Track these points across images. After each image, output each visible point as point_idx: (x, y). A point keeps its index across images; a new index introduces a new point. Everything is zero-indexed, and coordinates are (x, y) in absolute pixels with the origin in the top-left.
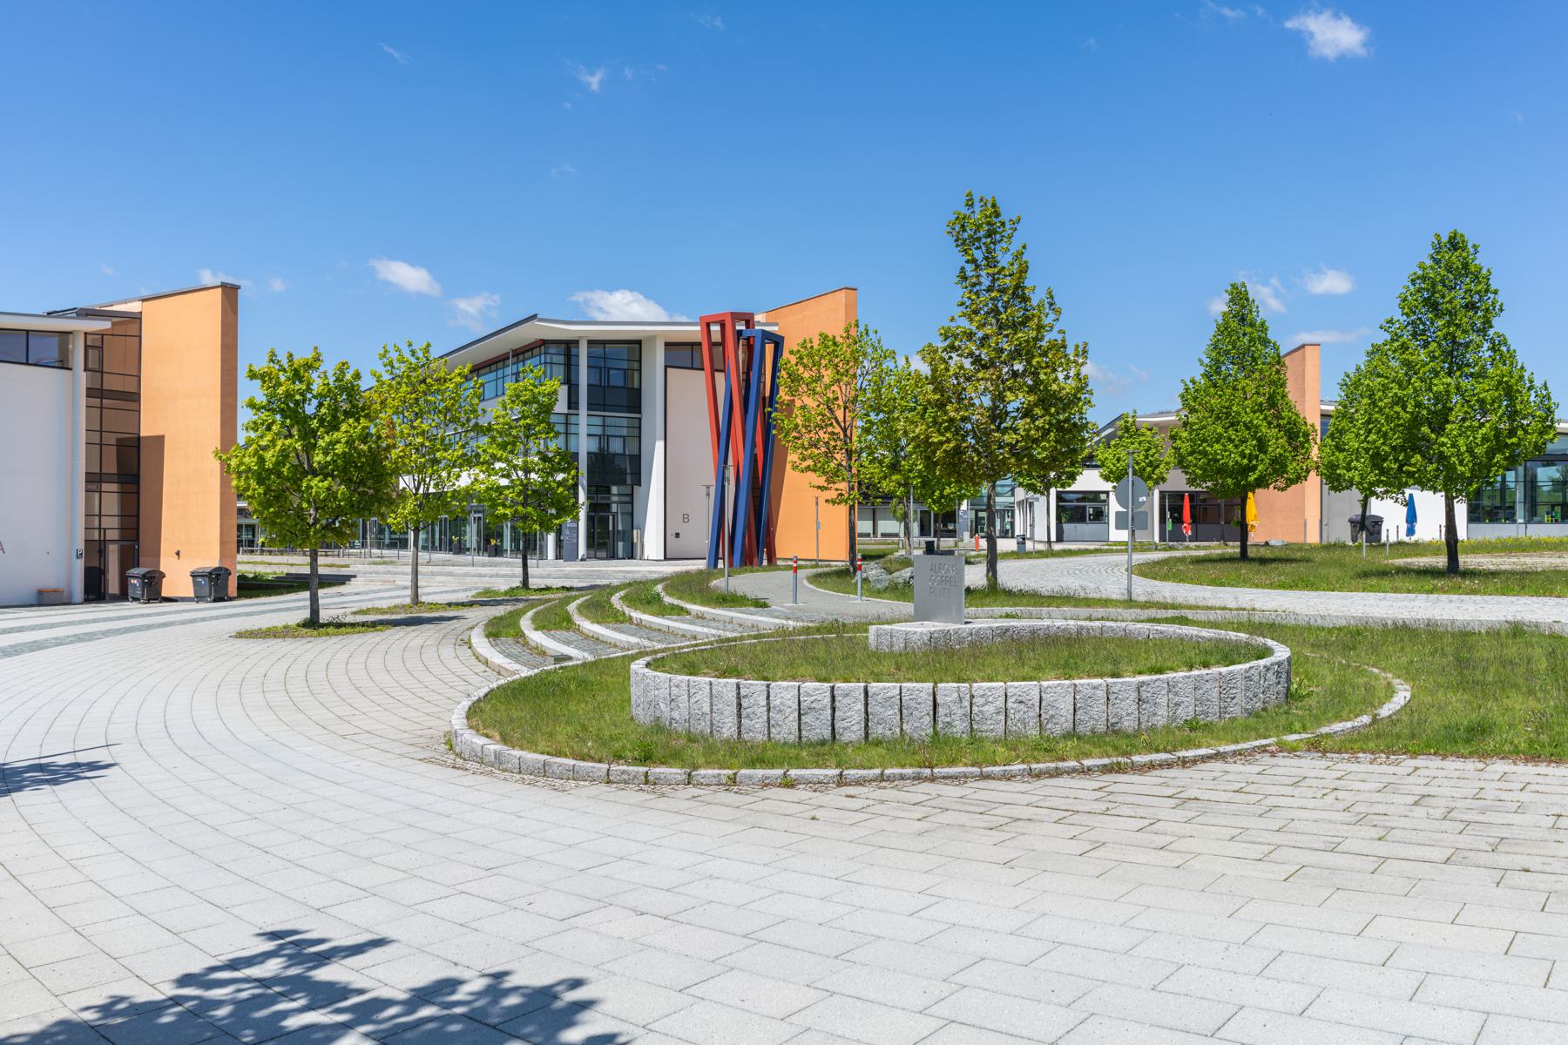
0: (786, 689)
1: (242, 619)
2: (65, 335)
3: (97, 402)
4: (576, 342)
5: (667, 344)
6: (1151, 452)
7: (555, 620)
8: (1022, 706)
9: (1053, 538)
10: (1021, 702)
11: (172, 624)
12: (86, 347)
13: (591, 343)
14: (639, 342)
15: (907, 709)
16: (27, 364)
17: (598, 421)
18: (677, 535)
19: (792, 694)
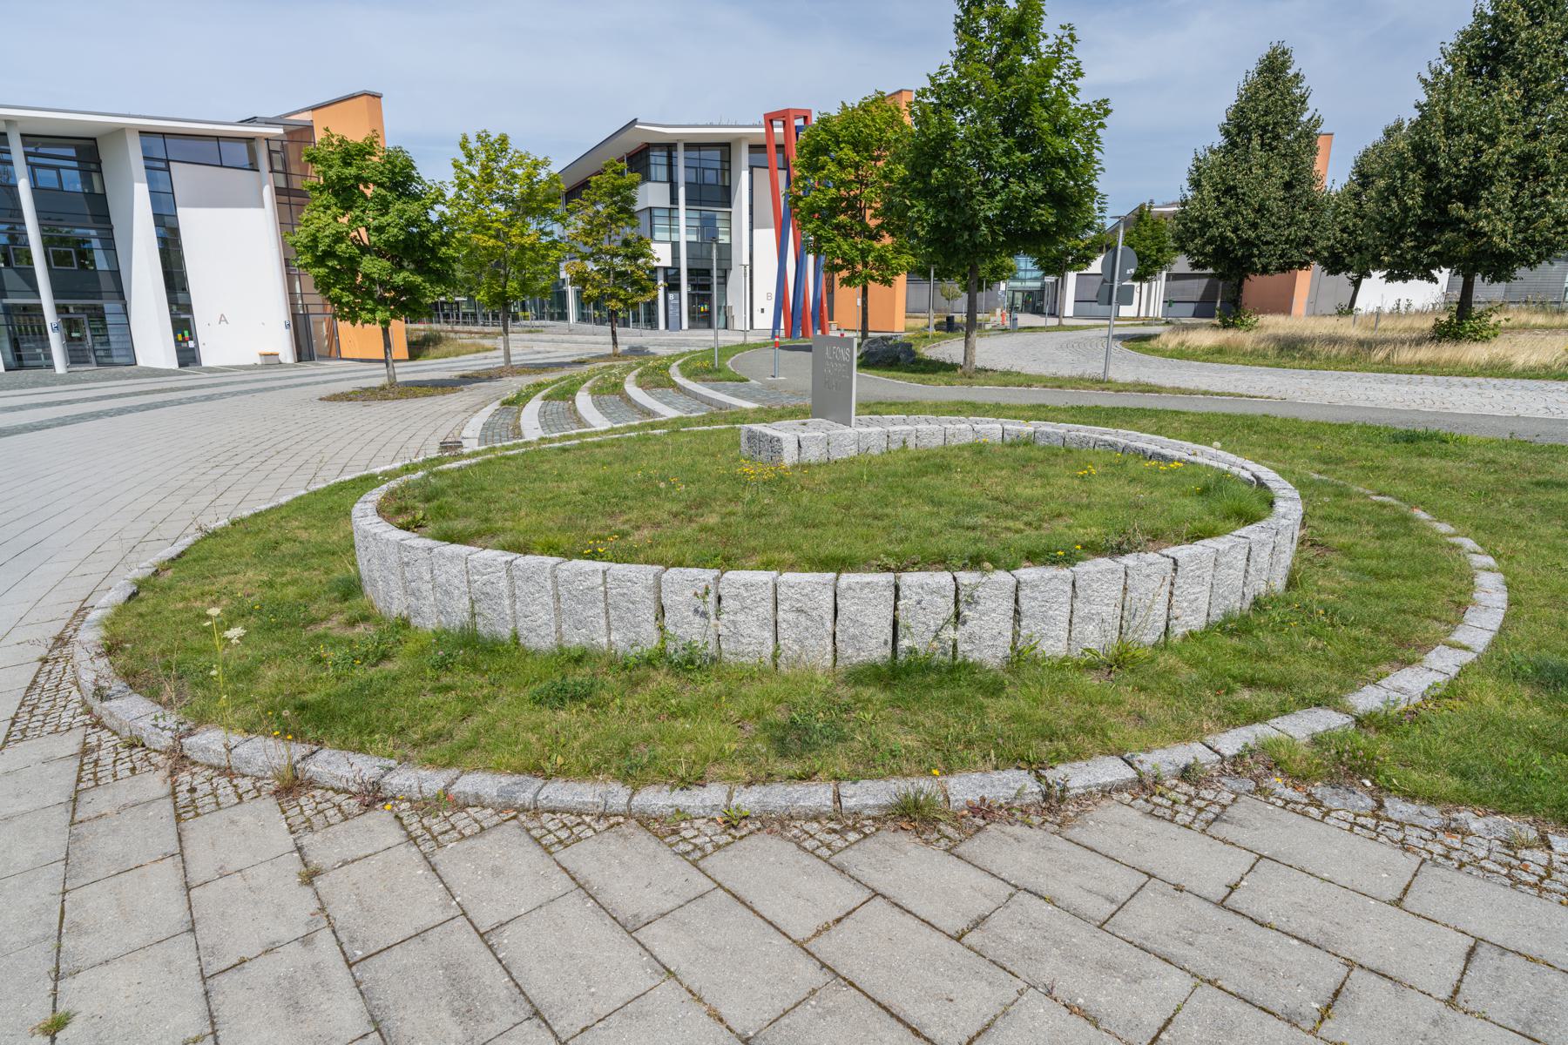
0: (452, 559)
1: (54, 408)
2: (250, 140)
3: (285, 199)
4: (675, 145)
5: (751, 147)
6: (1095, 586)
7: (656, 378)
8: (802, 618)
9: (1107, 322)
10: (799, 611)
11: (273, 389)
12: (270, 152)
13: (689, 146)
14: (728, 145)
15: (615, 609)
16: (221, 166)
17: (696, 215)
18: (763, 310)
19: (458, 568)
